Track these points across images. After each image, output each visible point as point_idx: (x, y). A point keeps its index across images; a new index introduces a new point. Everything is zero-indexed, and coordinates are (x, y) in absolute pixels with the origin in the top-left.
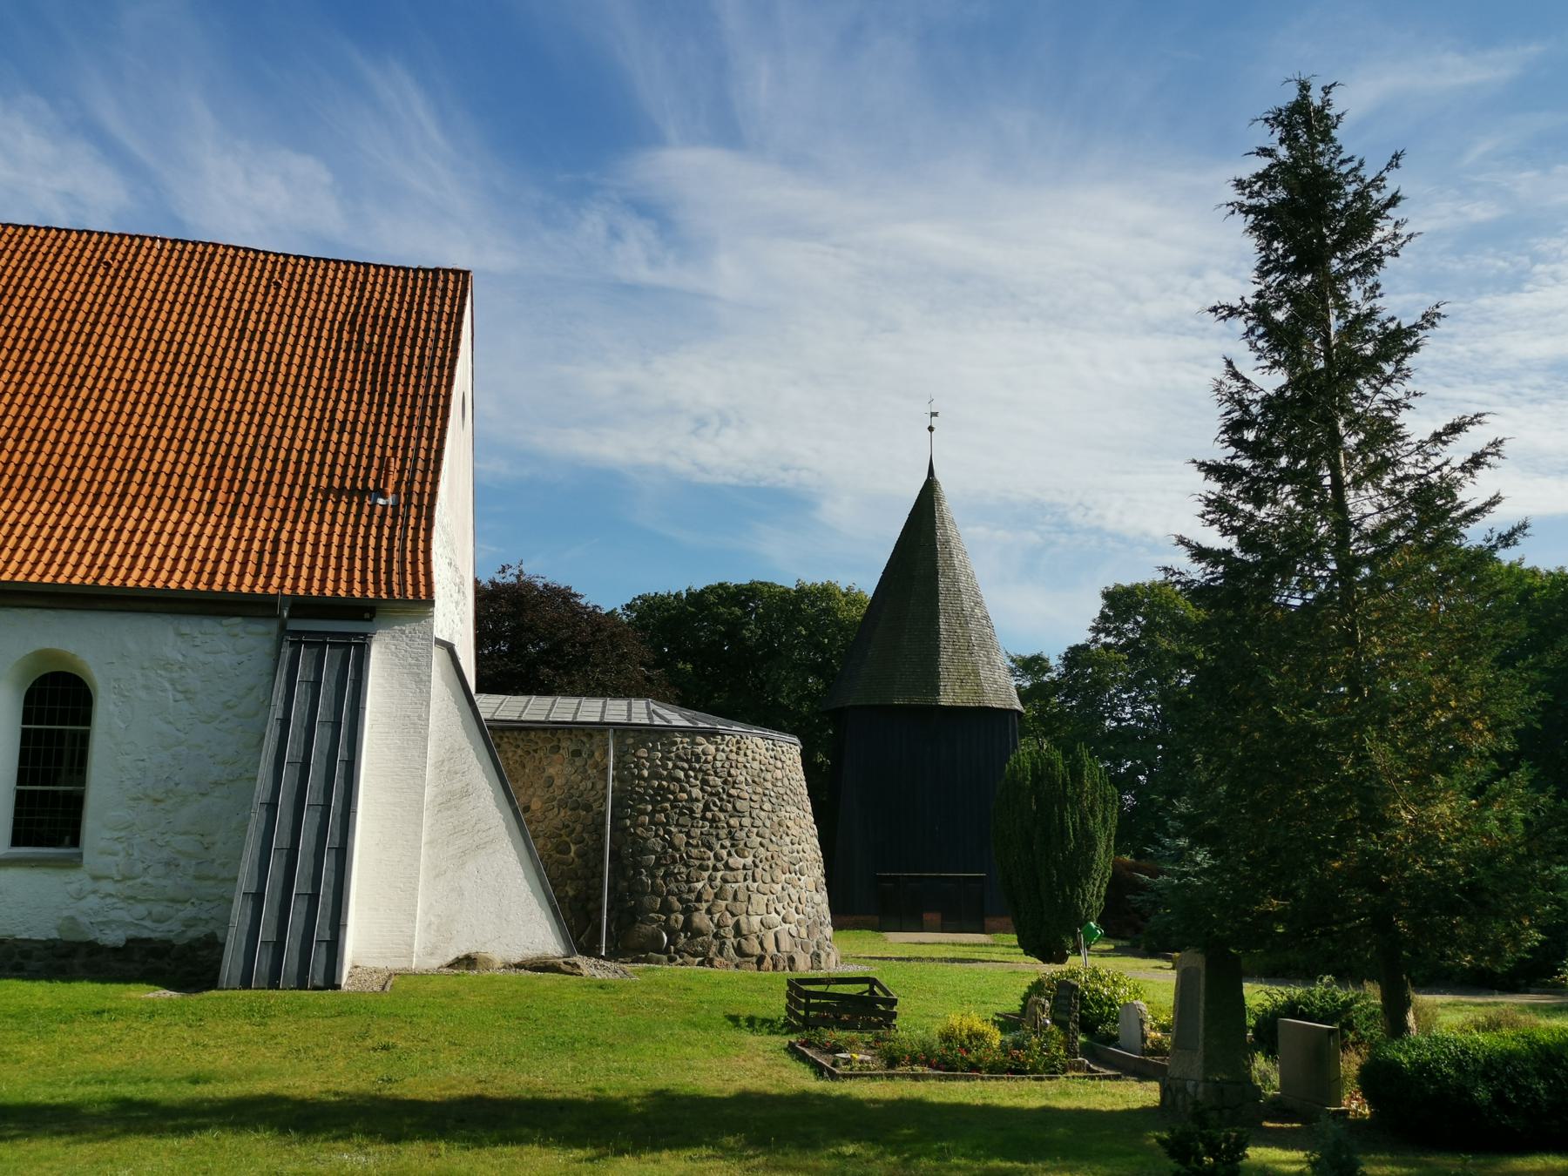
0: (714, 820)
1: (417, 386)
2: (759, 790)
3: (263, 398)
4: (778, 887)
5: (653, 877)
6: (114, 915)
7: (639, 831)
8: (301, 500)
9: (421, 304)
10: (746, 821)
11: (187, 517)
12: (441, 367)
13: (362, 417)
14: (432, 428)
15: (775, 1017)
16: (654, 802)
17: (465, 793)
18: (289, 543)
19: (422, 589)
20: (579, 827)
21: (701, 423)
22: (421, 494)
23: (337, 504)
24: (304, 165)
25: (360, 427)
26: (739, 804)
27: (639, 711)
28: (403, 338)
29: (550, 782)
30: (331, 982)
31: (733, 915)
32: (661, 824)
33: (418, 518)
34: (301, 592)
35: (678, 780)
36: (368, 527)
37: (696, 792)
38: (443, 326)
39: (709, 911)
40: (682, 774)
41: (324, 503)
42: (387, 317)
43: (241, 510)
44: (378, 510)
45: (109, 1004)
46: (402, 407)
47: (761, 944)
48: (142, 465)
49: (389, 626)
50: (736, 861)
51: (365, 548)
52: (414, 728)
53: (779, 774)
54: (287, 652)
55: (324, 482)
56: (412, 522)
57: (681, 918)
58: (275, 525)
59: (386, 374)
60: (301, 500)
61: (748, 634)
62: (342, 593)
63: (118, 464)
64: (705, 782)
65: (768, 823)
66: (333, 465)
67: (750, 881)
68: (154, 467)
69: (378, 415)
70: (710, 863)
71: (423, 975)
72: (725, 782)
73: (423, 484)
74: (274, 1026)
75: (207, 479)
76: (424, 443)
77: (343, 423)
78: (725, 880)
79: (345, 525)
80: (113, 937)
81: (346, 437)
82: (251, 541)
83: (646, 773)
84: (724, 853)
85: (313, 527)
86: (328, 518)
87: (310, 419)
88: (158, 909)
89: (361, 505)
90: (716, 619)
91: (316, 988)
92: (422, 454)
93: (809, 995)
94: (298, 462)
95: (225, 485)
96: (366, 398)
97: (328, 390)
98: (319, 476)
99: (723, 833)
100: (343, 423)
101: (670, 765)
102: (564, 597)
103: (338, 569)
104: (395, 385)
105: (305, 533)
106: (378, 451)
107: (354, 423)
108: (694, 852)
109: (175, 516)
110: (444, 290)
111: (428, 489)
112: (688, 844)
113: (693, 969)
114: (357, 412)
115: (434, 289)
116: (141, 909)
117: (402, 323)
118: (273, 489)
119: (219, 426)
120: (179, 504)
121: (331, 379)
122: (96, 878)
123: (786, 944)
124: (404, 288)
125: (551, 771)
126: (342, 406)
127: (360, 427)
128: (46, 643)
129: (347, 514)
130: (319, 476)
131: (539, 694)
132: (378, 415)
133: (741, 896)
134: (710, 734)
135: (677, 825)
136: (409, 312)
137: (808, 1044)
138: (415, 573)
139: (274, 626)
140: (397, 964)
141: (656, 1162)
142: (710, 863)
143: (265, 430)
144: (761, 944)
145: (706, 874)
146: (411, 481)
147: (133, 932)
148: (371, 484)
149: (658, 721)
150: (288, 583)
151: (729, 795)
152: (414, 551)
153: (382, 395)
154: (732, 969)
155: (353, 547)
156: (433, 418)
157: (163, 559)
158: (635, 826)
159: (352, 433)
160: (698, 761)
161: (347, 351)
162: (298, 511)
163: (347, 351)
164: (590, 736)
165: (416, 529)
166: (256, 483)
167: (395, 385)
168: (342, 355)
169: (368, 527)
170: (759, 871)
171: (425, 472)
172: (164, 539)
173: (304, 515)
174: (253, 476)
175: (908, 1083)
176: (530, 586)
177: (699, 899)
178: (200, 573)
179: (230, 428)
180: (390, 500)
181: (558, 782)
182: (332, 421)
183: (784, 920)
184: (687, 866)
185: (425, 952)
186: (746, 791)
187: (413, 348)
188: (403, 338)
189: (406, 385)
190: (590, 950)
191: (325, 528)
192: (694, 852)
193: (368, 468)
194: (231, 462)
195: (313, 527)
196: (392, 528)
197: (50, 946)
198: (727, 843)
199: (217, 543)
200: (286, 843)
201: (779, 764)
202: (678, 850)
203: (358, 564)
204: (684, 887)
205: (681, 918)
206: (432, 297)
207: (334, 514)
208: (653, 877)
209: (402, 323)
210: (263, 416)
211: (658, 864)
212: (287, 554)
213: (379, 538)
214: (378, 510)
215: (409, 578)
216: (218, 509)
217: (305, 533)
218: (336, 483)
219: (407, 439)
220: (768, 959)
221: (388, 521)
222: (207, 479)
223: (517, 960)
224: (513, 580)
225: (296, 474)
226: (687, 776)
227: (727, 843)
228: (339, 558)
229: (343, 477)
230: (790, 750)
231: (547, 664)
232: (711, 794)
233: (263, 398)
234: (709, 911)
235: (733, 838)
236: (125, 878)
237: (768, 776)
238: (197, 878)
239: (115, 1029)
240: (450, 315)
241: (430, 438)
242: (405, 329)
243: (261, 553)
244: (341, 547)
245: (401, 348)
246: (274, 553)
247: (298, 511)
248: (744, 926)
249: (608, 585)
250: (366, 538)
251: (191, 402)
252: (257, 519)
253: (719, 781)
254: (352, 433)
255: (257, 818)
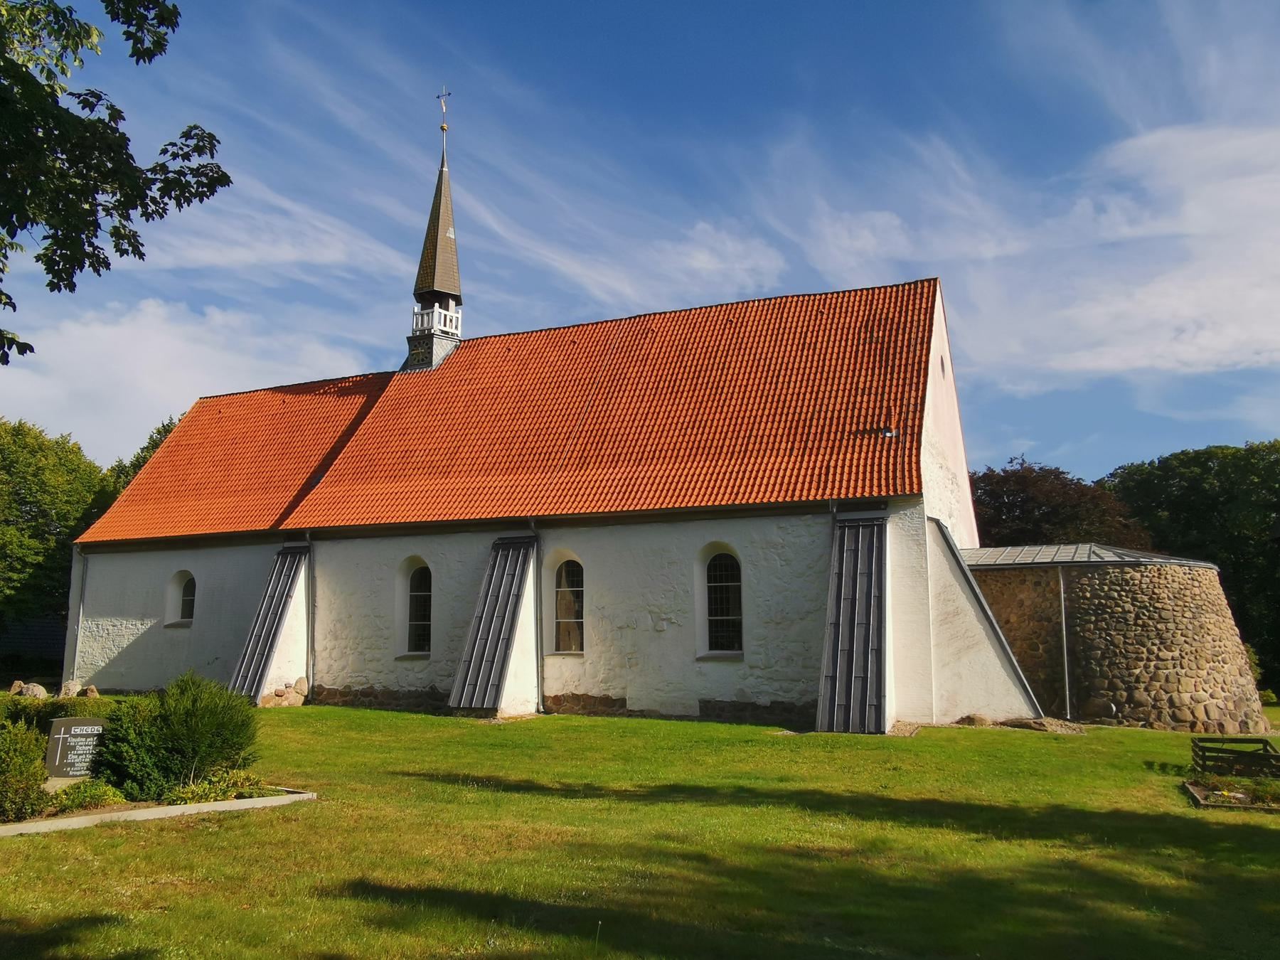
0: (1144, 626)
1: (907, 359)
2: (1180, 603)
3: (817, 382)
4: (1205, 673)
5: (1101, 666)
6: (765, 688)
7: (1087, 634)
8: (841, 441)
9: (907, 306)
10: (1172, 626)
11: (779, 459)
12: (922, 344)
13: (875, 384)
14: (918, 384)
15: (1183, 763)
16: (1096, 615)
17: (956, 613)
18: (835, 467)
19: (915, 486)
20: (1043, 633)
21: (1180, 330)
22: (913, 427)
23: (862, 440)
24: (885, 219)
25: (873, 390)
26: (1164, 614)
27: (1081, 553)
28: (897, 330)
29: (1021, 603)
30: (879, 729)
31: (1167, 692)
32: (1103, 629)
33: (912, 442)
34: (842, 496)
35: (1113, 599)
36: (881, 452)
37: (1128, 607)
38: (922, 317)
39: (1146, 689)
40: (1116, 594)
41: (855, 440)
42: (886, 319)
43: (808, 451)
44: (887, 440)
45: (757, 737)
46: (899, 373)
47: (1192, 713)
48: (754, 433)
49: (897, 512)
50: (1165, 654)
51: (880, 465)
52: (919, 573)
53: (1197, 591)
54: (838, 533)
55: (854, 428)
56: (908, 445)
57: (1125, 694)
58: (827, 457)
59: (888, 354)
60: (841, 441)
61: (1207, 486)
62: (866, 494)
63: (742, 434)
64: (1134, 599)
65: (1190, 627)
66: (859, 417)
67: (1178, 669)
68: (761, 433)
69: (884, 381)
70: (1144, 656)
71: (938, 728)
72: (1151, 598)
73: (913, 420)
74: (838, 753)
75: (788, 436)
76: (913, 394)
77: (863, 390)
78: (1157, 668)
79: (867, 453)
80: (764, 700)
81: (865, 398)
82: (814, 469)
83: (1088, 595)
84: (1155, 648)
85: (848, 456)
86: (857, 449)
87: (844, 391)
88: (785, 685)
89: (876, 439)
90: (1182, 477)
91: (870, 733)
92: (912, 401)
93: (1204, 749)
94: (839, 418)
95: (798, 437)
96: (877, 371)
97: (854, 371)
98: (851, 425)
99: (1152, 635)
100: (863, 390)
101: (1106, 588)
102: (1057, 474)
103: (864, 480)
104: (894, 360)
105: (844, 460)
106: (885, 404)
107: (870, 389)
108: (1130, 648)
109: (772, 460)
110: (922, 293)
111: (917, 422)
112: (1125, 643)
113: (1138, 729)
114: (872, 381)
115: (915, 295)
116: (776, 685)
117: (896, 320)
118: (825, 435)
119: (793, 404)
120: (775, 452)
121: (855, 364)
122: (751, 667)
123: (1215, 714)
124: (896, 298)
125: (1022, 596)
126: (862, 379)
127: (873, 390)
128: (410, 554)
129: (868, 446)
130: (851, 425)
131: (1065, 544)
132: (884, 381)
133: (1171, 679)
134: (1135, 565)
135: (1115, 630)
136: (900, 313)
137: (1195, 784)
138: (911, 477)
139: (829, 518)
140: (925, 721)
141: (1021, 846)
142: (1144, 656)
143: (819, 402)
144: (1192, 713)
145: (1142, 664)
146: (906, 419)
147: (773, 698)
148: (882, 425)
149: (1094, 558)
150: (836, 492)
151: (1156, 608)
152: (910, 463)
153: (886, 368)
154: (1169, 730)
155: (872, 465)
156: (918, 377)
157: (767, 485)
158: (1083, 631)
159: (869, 395)
160: (1127, 584)
161: (864, 345)
162: (840, 448)
163: (864, 345)
164: (1046, 572)
165: (910, 449)
166: (815, 434)
167: (894, 360)
168: (861, 348)
169: (881, 452)
170: (1185, 662)
171: (914, 413)
172: (767, 474)
173: (843, 449)
174: (813, 430)
175: (1262, 814)
176: (1031, 470)
177: (1138, 680)
178: (787, 491)
179: (800, 403)
180: (894, 433)
181: (1027, 603)
182: (857, 389)
183: (1212, 696)
184: (1126, 658)
185: (941, 713)
186: (1169, 604)
187: (903, 335)
188: (897, 330)
189: (901, 359)
190: (1059, 715)
191: (856, 456)
192: (1130, 648)
193: (880, 416)
194: (801, 424)
195: (848, 456)
196: (896, 451)
197: (733, 705)
198: (1157, 642)
199: (795, 472)
200: (847, 647)
201: (1196, 584)
202: (1117, 647)
203: (876, 475)
204: (1125, 673)
205: (1125, 694)
206: (914, 300)
207: (861, 446)
208: (1101, 666)
209: (896, 320)
210: (817, 393)
211: (1103, 657)
212: (834, 475)
213: (888, 458)
214: (887, 440)
215: (907, 481)
216: (795, 453)
217: (844, 460)
218: (861, 427)
219: (903, 393)
220: (1199, 724)
221: (893, 446)
222: (788, 436)
223: (1002, 720)
224: (1018, 467)
225: (837, 426)
226: (1120, 596)
227: (1157, 642)
228: (864, 473)
229: (865, 423)
230: (1208, 575)
231: (1048, 522)
232: (1140, 607)
233: (817, 382)
234: (1146, 689)
235: (1161, 638)
236: (766, 668)
237: (1188, 593)
238: (805, 667)
239: (751, 750)
240: (926, 309)
241: (917, 390)
242: (898, 324)
243: (820, 475)
244: (865, 466)
245: (897, 336)
246: (827, 475)
247: (840, 448)
248: (1176, 700)
249: (1089, 462)
250: (880, 458)
251: (778, 392)
252: (817, 455)
253: (1146, 598)
254: (869, 395)
255: (829, 631)
